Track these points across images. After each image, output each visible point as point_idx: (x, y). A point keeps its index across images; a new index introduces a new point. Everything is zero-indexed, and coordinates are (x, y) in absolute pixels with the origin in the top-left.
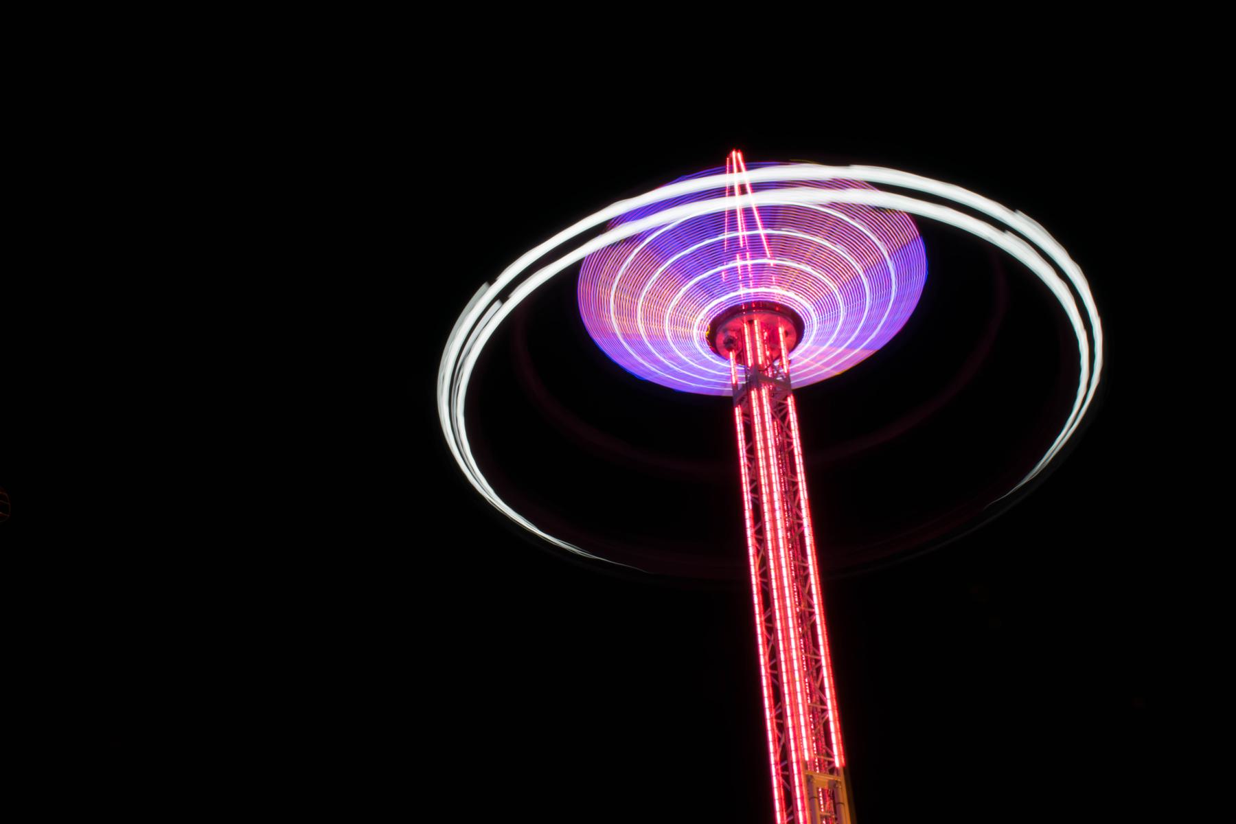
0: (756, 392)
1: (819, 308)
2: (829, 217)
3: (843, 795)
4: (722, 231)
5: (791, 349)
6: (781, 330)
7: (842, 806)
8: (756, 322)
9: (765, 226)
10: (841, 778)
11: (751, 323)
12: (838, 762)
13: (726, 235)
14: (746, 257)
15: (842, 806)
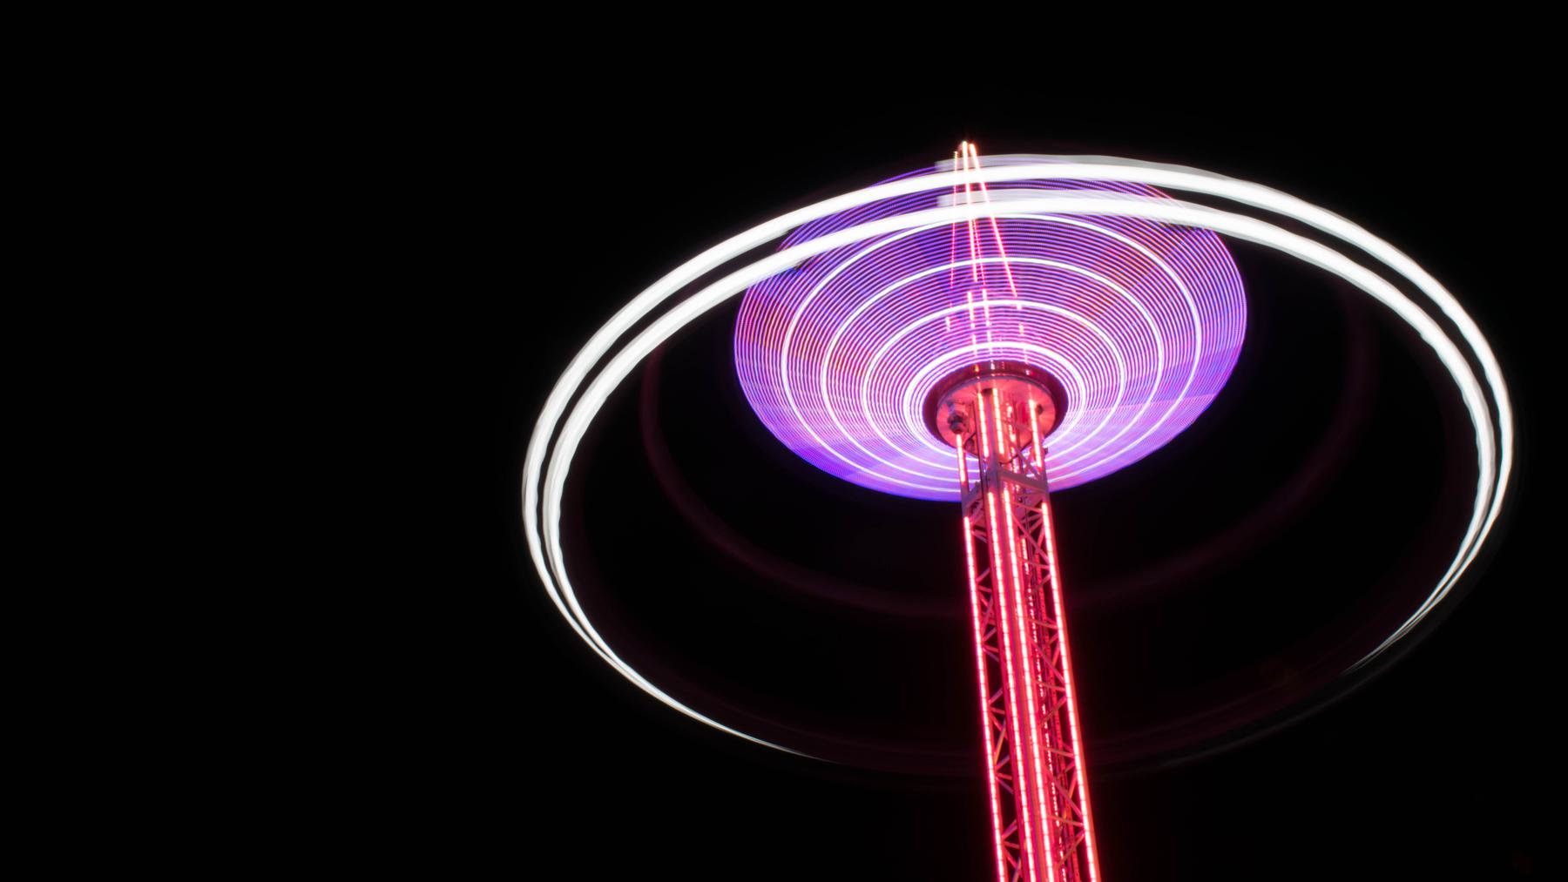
0: (994, 496)
5: (1046, 433)
8: (995, 391)
9: (1009, 252)
11: (987, 392)
13: (954, 265)
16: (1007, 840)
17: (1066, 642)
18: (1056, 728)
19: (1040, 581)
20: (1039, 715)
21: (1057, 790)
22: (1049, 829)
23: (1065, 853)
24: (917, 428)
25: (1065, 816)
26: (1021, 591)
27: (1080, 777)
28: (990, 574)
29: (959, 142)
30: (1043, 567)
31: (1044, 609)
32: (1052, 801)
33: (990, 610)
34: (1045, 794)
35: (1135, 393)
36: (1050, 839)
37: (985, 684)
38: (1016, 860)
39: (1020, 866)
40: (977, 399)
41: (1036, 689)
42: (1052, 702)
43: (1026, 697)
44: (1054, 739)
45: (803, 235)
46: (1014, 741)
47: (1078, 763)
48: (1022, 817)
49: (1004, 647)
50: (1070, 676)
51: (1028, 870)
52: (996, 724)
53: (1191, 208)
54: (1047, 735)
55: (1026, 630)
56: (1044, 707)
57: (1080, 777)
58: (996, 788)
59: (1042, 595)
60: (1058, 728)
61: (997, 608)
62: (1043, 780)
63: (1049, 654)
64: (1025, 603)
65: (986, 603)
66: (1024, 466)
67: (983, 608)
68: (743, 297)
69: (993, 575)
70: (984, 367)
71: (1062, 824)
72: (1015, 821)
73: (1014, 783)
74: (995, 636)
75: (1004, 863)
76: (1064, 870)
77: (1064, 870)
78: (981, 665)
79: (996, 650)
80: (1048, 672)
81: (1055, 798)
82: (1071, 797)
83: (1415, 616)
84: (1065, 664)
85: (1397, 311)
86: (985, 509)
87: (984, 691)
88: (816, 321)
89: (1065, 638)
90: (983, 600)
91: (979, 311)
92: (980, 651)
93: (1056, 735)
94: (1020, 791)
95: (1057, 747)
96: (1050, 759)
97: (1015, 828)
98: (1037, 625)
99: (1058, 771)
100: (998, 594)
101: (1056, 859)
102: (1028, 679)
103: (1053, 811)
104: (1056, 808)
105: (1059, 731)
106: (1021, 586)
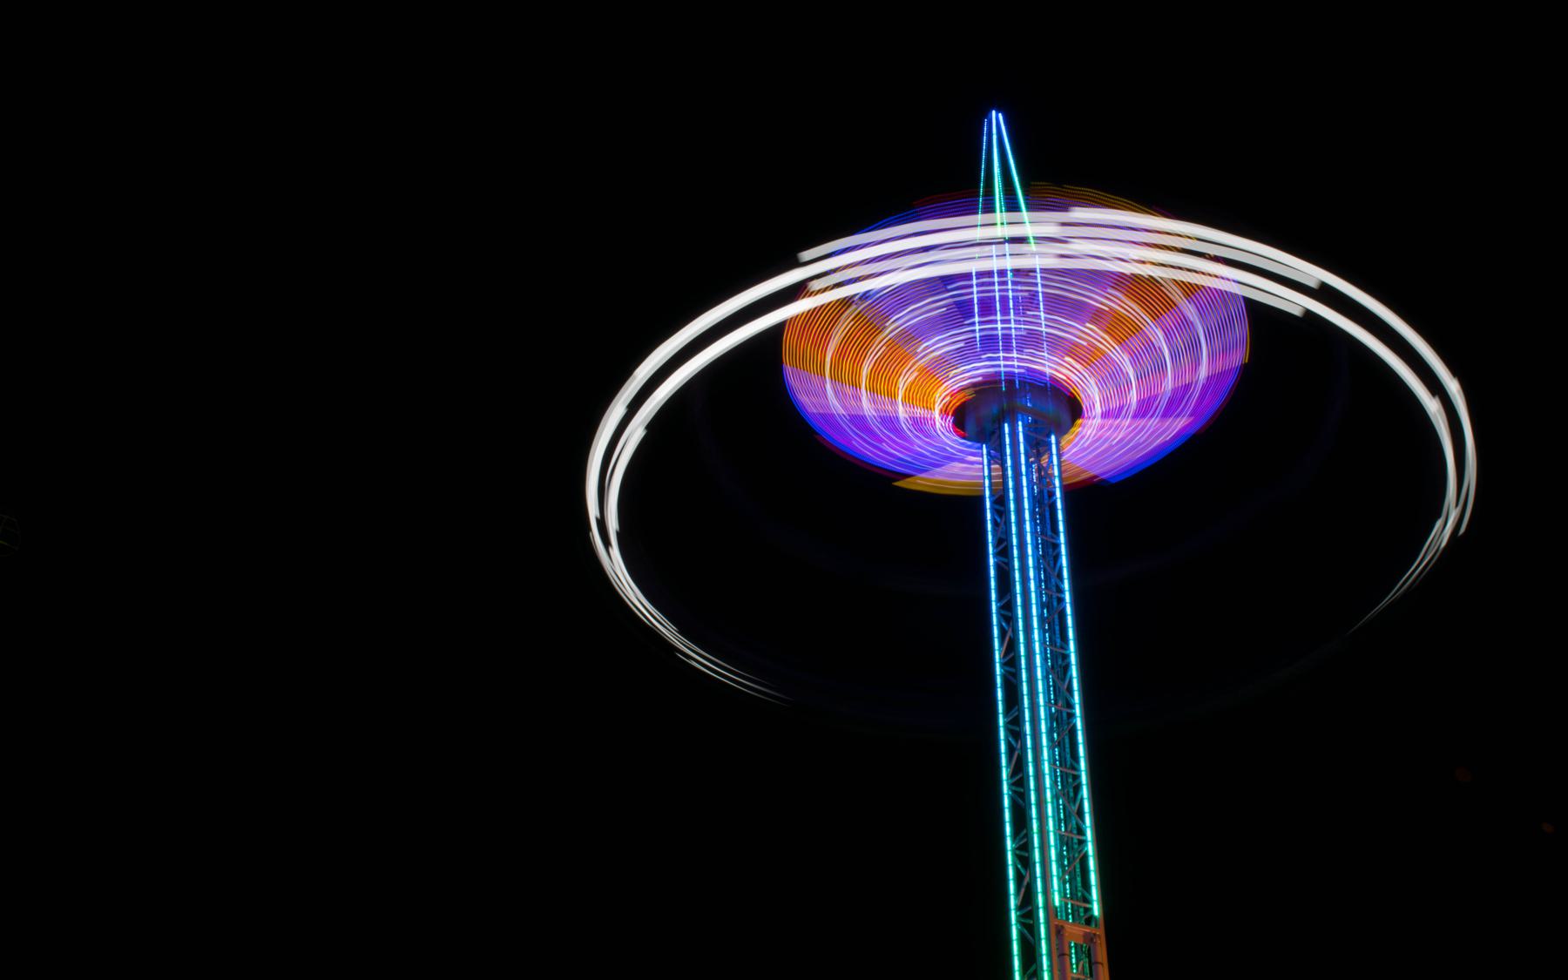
0: (1009, 426)
7: (1100, 966)
12: (1096, 910)
15: (1100, 966)
16: (1014, 784)
17: (1076, 652)
18: (1054, 622)
19: (1046, 502)
20: (1041, 617)
21: (1054, 681)
22: (1046, 715)
23: (1058, 736)
24: (941, 424)
25: (1060, 703)
26: (1029, 509)
27: (1074, 671)
28: (1006, 546)
29: (987, 114)
30: (1069, 711)
31: (1049, 526)
32: (1049, 691)
33: (1002, 526)
34: (1043, 685)
35: (1144, 409)
36: (1046, 723)
37: (1009, 808)
39: (1019, 746)
41: (1039, 596)
42: (1053, 605)
43: (1040, 729)
44: (1053, 638)
46: (1019, 640)
47: (1073, 659)
48: (1023, 703)
49: (1013, 558)
50: (1098, 893)
51: (1026, 749)
52: (1004, 624)
54: (1068, 886)
55: (1032, 543)
56: (1045, 611)
57: (1074, 671)
58: (1001, 678)
59: (1048, 514)
60: (1057, 628)
61: (1008, 523)
62: (1042, 672)
63: (1052, 565)
64: (1033, 519)
65: (999, 520)
66: (1043, 473)
67: (995, 523)
68: (785, 325)
69: (1013, 601)
71: (1057, 711)
72: (1017, 707)
74: (1021, 779)
75: (1005, 743)
76: (1056, 749)
77: (1056, 749)
78: (992, 573)
79: (1005, 560)
80: (1061, 693)
81: (1052, 689)
82: (1066, 687)
83: (1387, 598)
84: (1065, 574)
85: (1415, 392)
86: (1002, 436)
87: (994, 596)
89: (1079, 686)
90: (1004, 624)
91: (1003, 329)
92: (992, 561)
93: (1064, 750)
94: (1030, 804)
95: (1046, 536)
96: (1057, 757)
97: (1017, 713)
98: (1042, 540)
99: (1055, 666)
100: (1010, 512)
101: (1050, 739)
102: (1029, 538)
103: (1050, 700)
104: (1052, 697)
105: (1057, 632)
106: (1029, 506)
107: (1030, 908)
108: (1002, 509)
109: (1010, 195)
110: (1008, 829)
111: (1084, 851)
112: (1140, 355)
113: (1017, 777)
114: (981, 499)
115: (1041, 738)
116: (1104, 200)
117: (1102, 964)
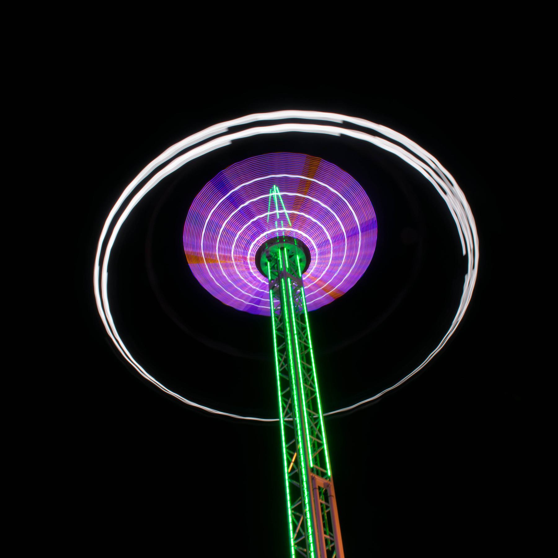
0: (284, 280)
1: (319, 246)
2: (329, 213)
3: (332, 492)
4: (267, 212)
5: (305, 270)
6: (298, 258)
7: (333, 497)
8: (285, 249)
9: (288, 208)
10: (332, 484)
11: (282, 249)
12: (329, 473)
14: (281, 226)
15: (333, 497)
18: (306, 358)
38: (288, 399)
40: (278, 252)
45: (209, 202)
49: (302, 481)
53: (326, 131)
70: (281, 238)
73: (282, 310)
88: (210, 205)
107: (294, 441)
108: (283, 333)
109: (272, 201)
110: (288, 497)
111: (323, 448)
112: (266, 200)
113: (291, 443)
114: (270, 318)
115: (302, 402)
116: (347, 197)
117: (333, 496)
